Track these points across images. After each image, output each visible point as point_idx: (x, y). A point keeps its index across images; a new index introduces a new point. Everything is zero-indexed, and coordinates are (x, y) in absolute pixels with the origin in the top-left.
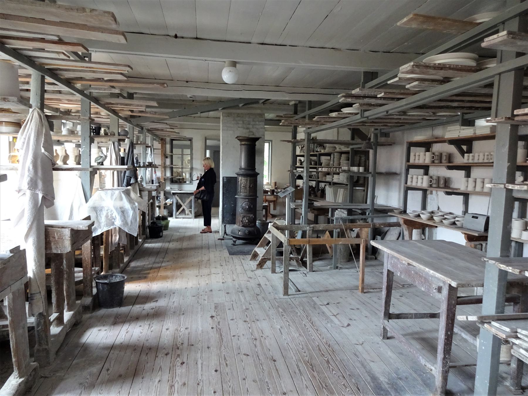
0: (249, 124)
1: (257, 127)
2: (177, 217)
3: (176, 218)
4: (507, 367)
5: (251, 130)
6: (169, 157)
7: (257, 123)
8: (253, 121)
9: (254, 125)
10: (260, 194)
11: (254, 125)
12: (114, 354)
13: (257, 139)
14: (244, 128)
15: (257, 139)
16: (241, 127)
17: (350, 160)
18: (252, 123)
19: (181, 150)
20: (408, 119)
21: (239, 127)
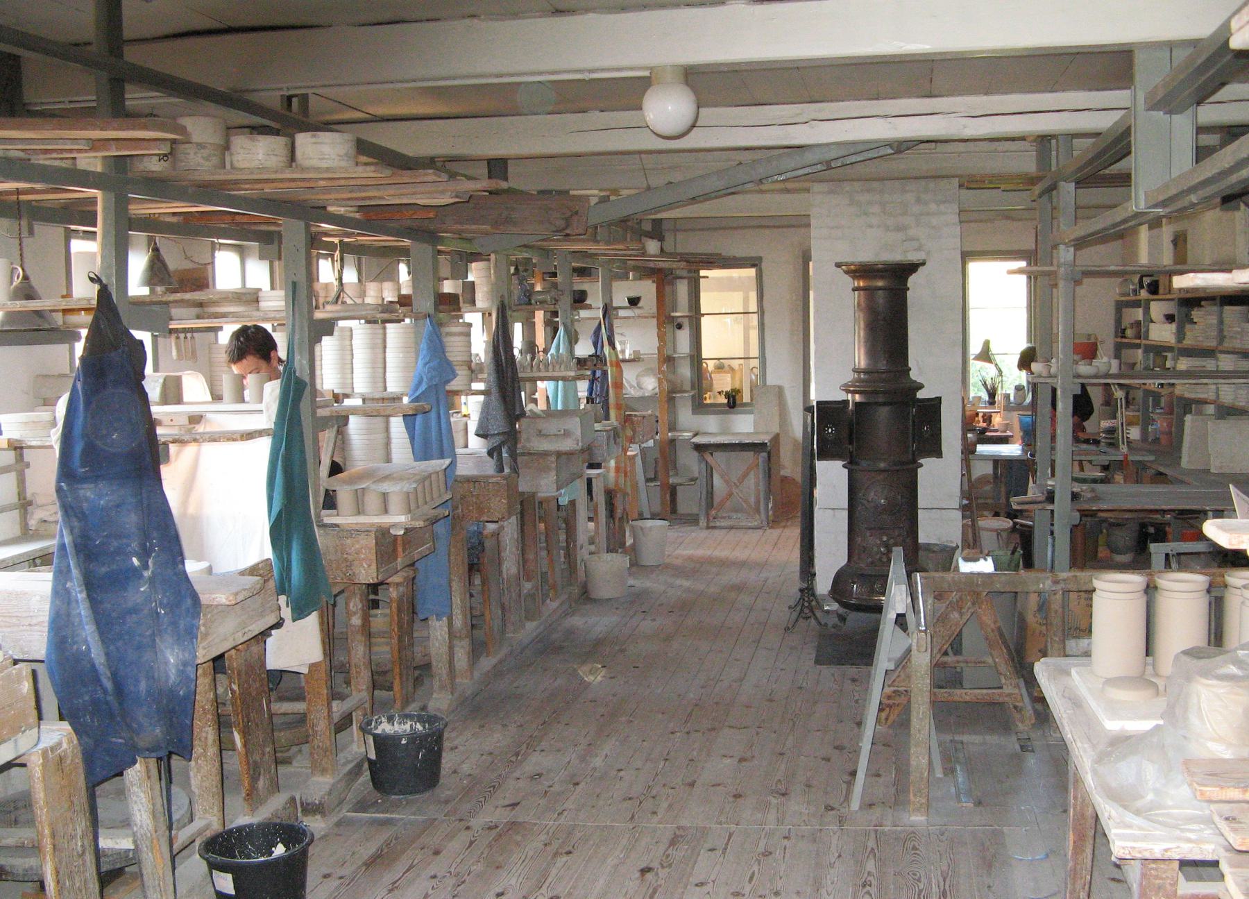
0: (905, 214)
1: (934, 221)
2: (712, 524)
3: (708, 528)
4: (466, 833)
5: (912, 232)
6: (686, 323)
7: (933, 207)
8: (918, 200)
9: (921, 214)
10: (155, 299)
11: (921, 214)
12: (178, 548)
13: (912, 268)
14: (887, 229)
15: (912, 268)
16: (879, 226)
17: (1172, 381)
18: (916, 209)
19: (756, 310)
20: (310, 179)
21: (871, 226)
